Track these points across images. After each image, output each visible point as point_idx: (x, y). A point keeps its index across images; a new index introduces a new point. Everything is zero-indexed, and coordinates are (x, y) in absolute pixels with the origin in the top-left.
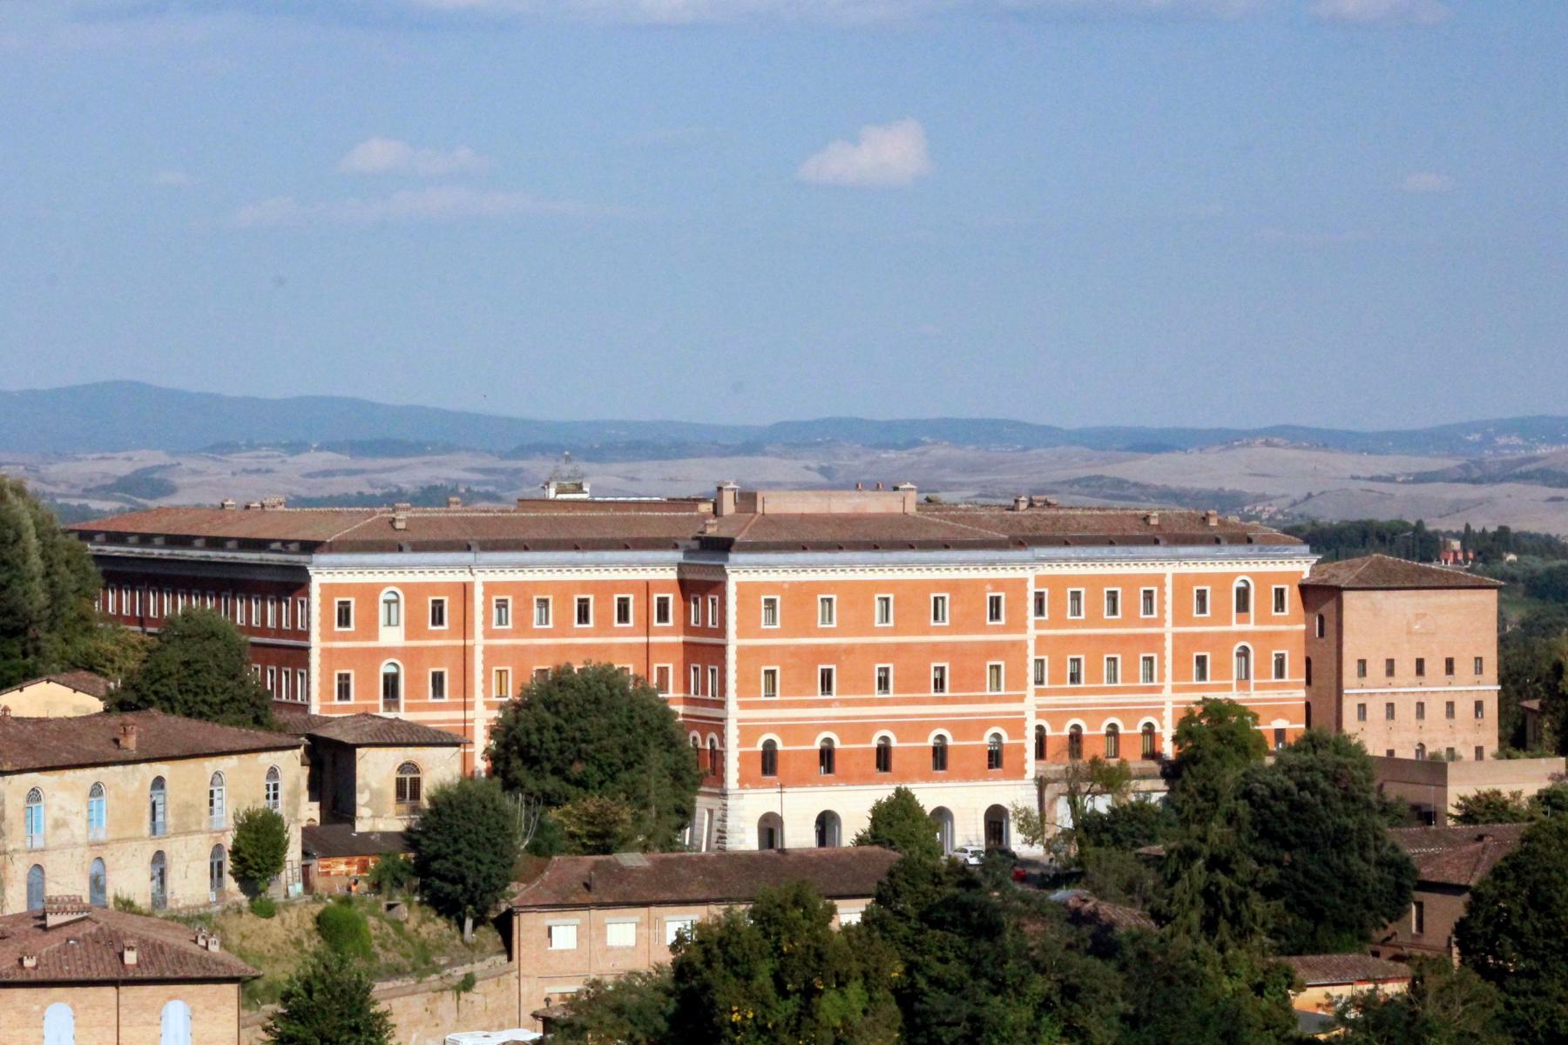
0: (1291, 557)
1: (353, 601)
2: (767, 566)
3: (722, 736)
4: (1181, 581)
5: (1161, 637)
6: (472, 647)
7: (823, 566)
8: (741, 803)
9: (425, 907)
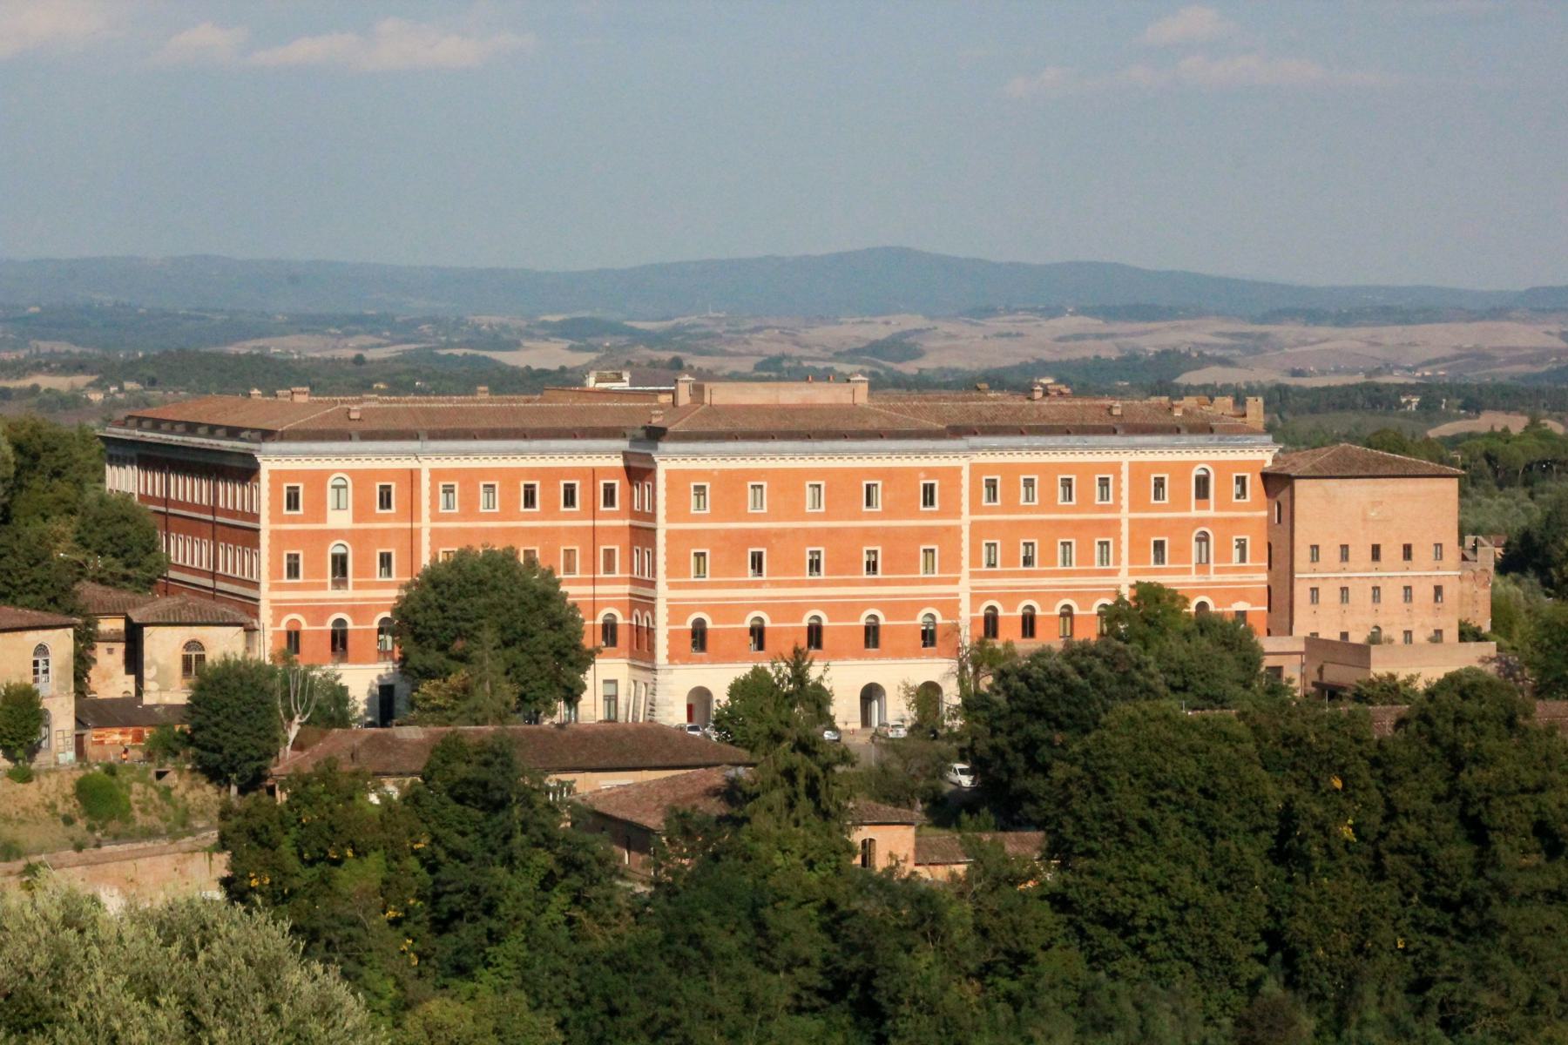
0: (1252, 446)
1: (301, 486)
2: (696, 455)
3: (653, 614)
4: (1137, 470)
5: (1117, 523)
6: (419, 530)
7: (752, 455)
8: (670, 677)
9: (197, 774)
